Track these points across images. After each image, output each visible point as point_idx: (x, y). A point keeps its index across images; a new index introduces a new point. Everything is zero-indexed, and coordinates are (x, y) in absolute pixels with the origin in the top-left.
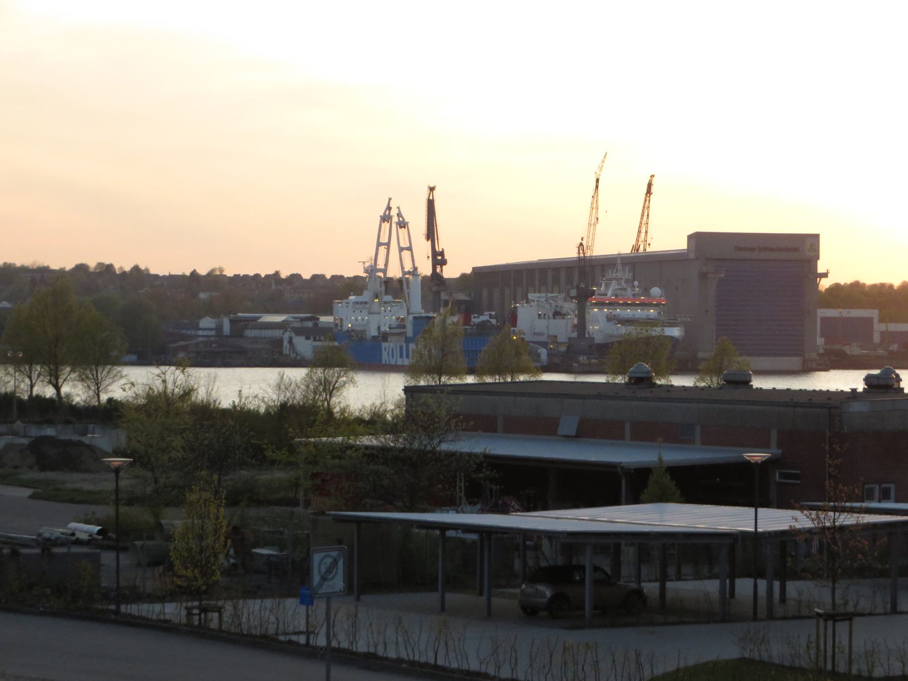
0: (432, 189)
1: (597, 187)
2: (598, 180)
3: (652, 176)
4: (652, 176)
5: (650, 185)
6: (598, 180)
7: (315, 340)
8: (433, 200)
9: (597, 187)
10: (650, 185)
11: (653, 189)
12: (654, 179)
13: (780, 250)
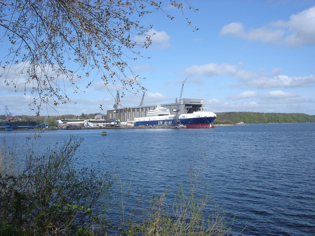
1: (183, 86)
2: (183, 85)
6: (183, 85)
7: (93, 123)
8: (118, 94)
9: (183, 86)
13: (197, 102)
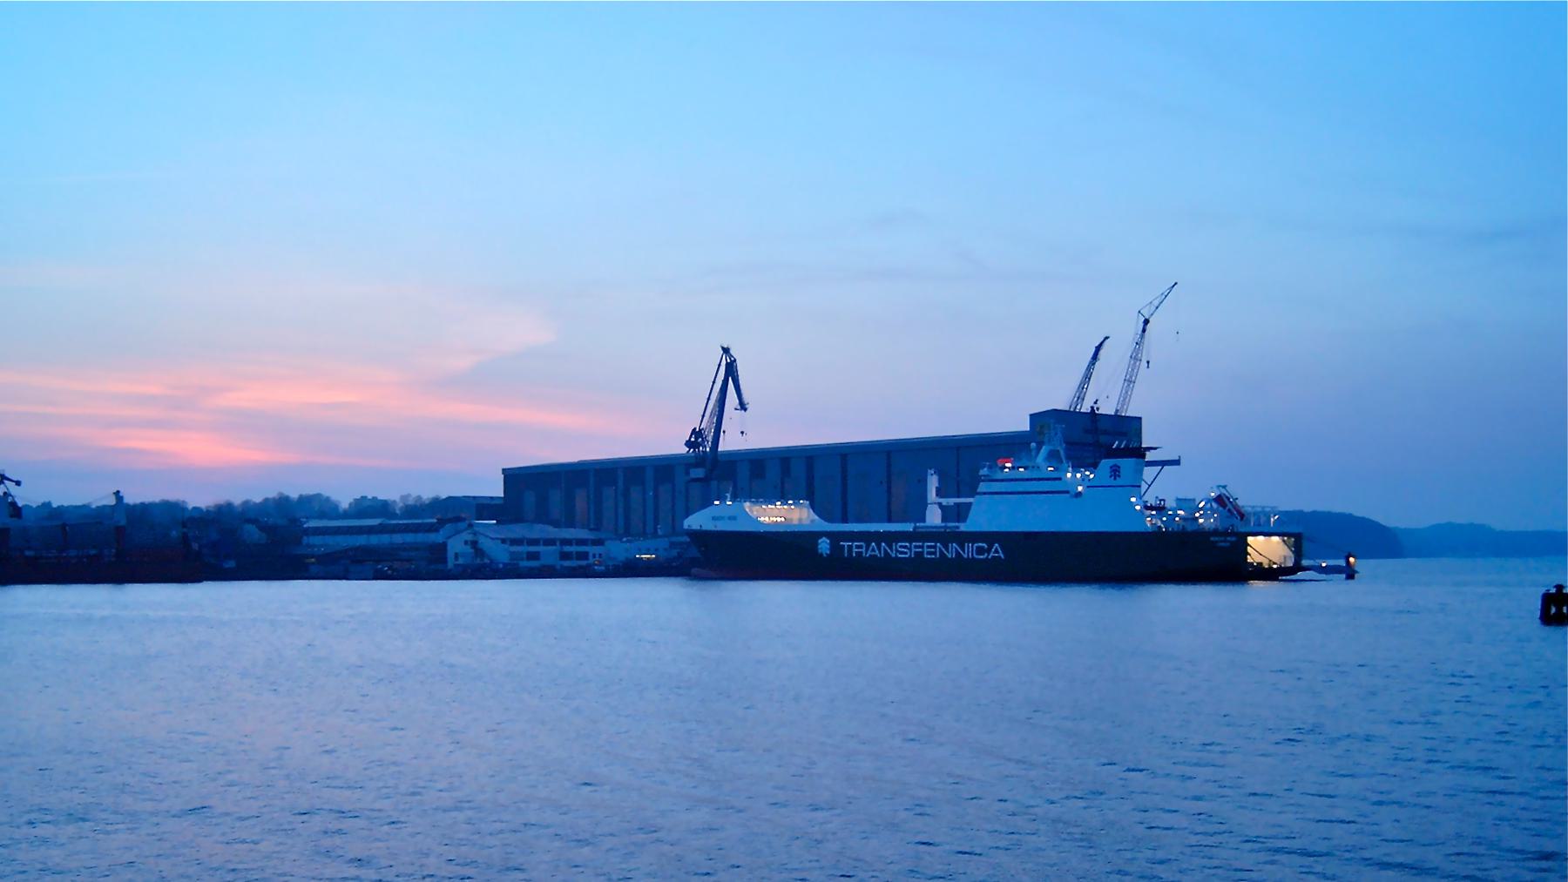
0: (726, 351)
1: (1144, 331)
2: (1146, 322)
3: (1107, 338)
4: (1107, 338)
5: (1098, 349)
6: (1146, 322)
9: (1144, 331)
10: (1098, 349)
11: (1102, 352)
12: (1107, 341)
